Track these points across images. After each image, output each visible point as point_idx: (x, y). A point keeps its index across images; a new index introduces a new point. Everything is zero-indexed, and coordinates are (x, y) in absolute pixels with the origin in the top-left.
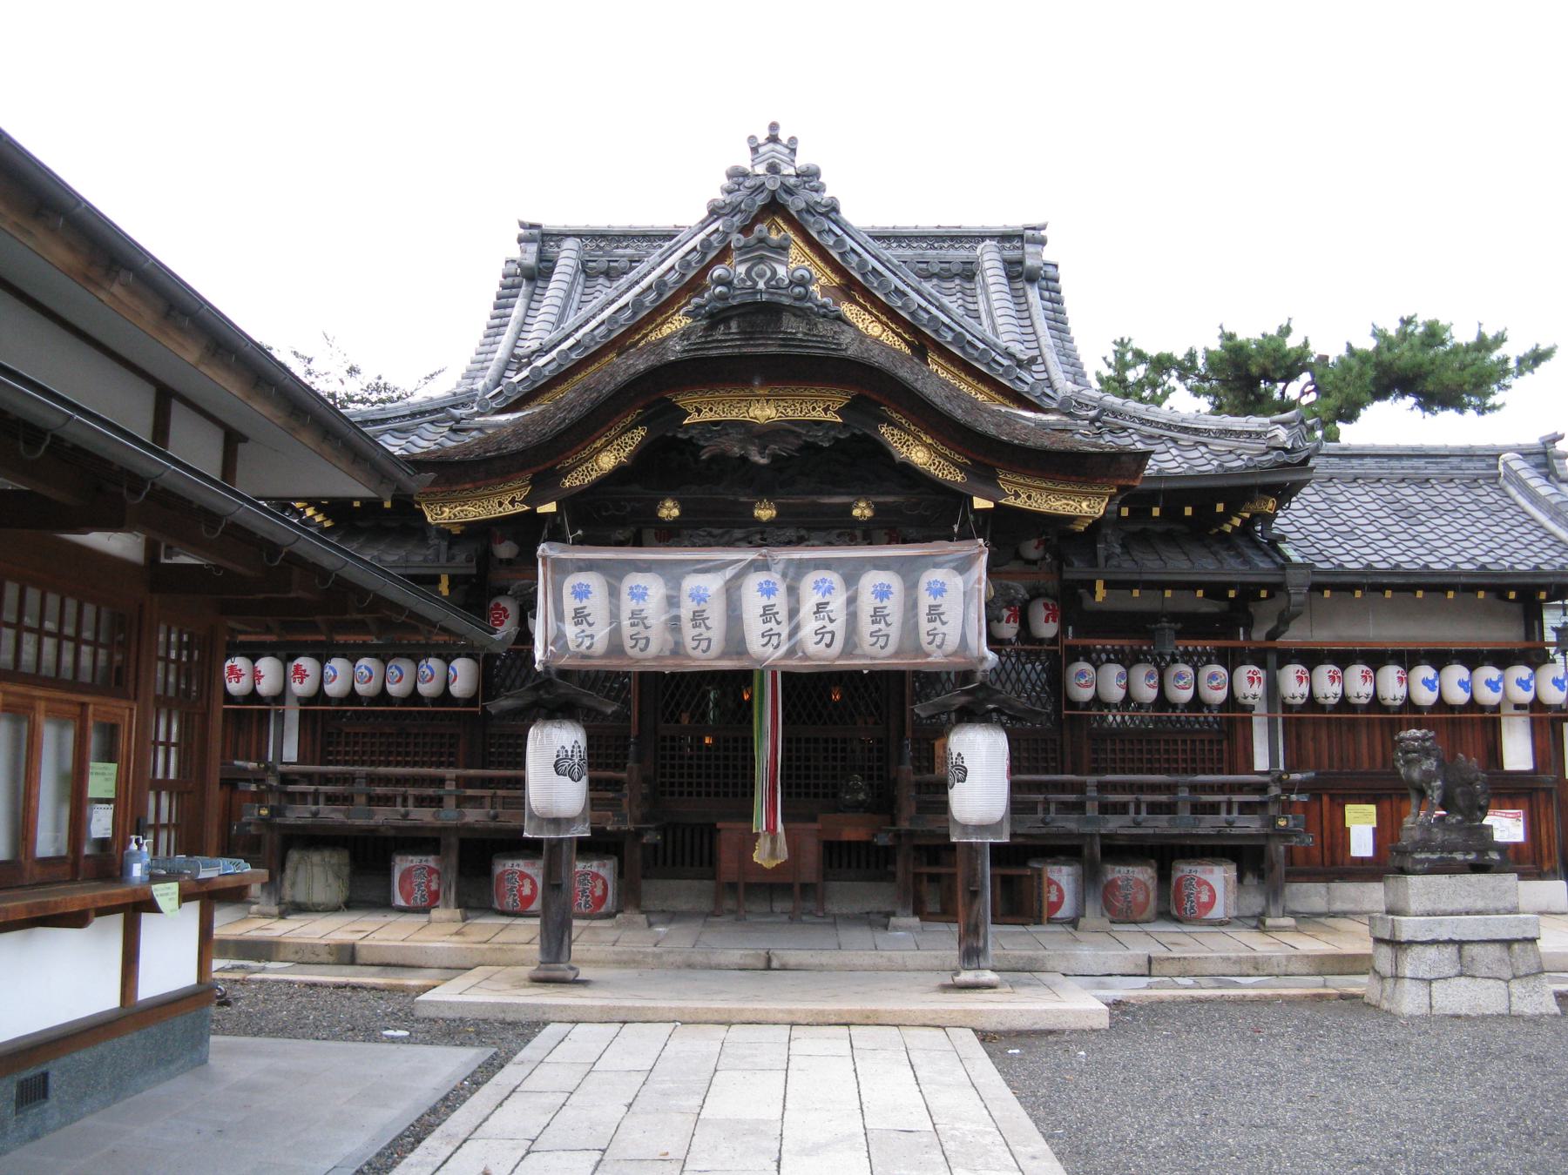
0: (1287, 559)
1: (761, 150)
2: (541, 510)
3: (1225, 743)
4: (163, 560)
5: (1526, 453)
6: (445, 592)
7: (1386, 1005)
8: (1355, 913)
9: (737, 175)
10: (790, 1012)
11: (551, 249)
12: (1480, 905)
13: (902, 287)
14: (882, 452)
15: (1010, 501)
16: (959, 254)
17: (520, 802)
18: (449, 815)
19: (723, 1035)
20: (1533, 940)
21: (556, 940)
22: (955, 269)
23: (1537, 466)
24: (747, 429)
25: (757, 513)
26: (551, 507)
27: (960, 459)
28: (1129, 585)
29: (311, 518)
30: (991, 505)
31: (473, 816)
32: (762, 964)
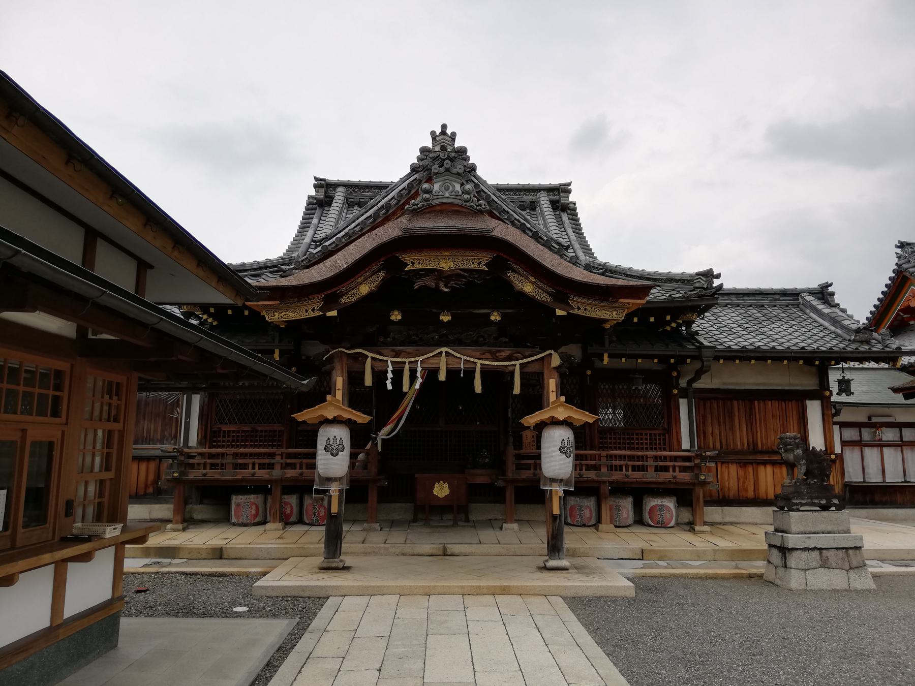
0: (702, 344)
1: (437, 139)
2: (329, 314)
3: (667, 436)
4: (90, 336)
5: (812, 292)
6: (277, 358)
7: (779, 582)
8: (736, 523)
9: (424, 150)
10: (462, 587)
11: (331, 192)
12: (829, 528)
13: (507, 209)
14: (509, 285)
15: (576, 312)
16: (528, 198)
17: (313, 466)
18: (277, 473)
19: (426, 604)
20: (860, 548)
21: (333, 543)
22: (526, 204)
23: (819, 299)
24: (439, 274)
25: (442, 318)
26: (334, 313)
27: (549, 289)
28: (620, 356)
29: (206, 320)
30: (565, 313)
31: (290, 473)
32: (441, 552)
